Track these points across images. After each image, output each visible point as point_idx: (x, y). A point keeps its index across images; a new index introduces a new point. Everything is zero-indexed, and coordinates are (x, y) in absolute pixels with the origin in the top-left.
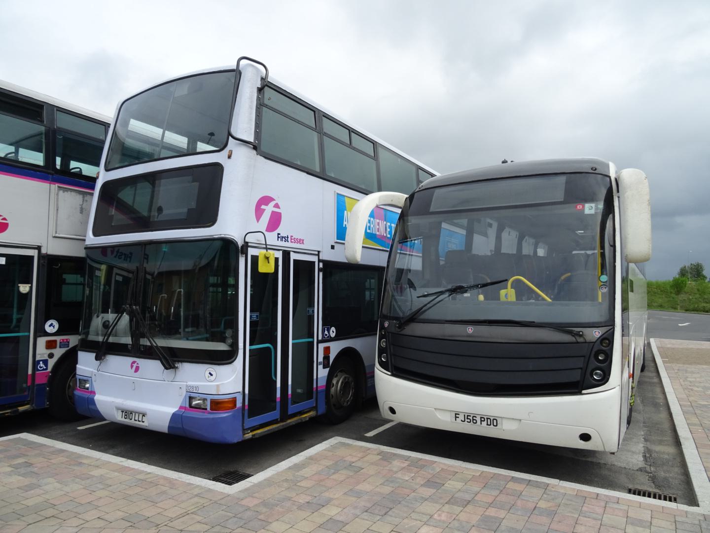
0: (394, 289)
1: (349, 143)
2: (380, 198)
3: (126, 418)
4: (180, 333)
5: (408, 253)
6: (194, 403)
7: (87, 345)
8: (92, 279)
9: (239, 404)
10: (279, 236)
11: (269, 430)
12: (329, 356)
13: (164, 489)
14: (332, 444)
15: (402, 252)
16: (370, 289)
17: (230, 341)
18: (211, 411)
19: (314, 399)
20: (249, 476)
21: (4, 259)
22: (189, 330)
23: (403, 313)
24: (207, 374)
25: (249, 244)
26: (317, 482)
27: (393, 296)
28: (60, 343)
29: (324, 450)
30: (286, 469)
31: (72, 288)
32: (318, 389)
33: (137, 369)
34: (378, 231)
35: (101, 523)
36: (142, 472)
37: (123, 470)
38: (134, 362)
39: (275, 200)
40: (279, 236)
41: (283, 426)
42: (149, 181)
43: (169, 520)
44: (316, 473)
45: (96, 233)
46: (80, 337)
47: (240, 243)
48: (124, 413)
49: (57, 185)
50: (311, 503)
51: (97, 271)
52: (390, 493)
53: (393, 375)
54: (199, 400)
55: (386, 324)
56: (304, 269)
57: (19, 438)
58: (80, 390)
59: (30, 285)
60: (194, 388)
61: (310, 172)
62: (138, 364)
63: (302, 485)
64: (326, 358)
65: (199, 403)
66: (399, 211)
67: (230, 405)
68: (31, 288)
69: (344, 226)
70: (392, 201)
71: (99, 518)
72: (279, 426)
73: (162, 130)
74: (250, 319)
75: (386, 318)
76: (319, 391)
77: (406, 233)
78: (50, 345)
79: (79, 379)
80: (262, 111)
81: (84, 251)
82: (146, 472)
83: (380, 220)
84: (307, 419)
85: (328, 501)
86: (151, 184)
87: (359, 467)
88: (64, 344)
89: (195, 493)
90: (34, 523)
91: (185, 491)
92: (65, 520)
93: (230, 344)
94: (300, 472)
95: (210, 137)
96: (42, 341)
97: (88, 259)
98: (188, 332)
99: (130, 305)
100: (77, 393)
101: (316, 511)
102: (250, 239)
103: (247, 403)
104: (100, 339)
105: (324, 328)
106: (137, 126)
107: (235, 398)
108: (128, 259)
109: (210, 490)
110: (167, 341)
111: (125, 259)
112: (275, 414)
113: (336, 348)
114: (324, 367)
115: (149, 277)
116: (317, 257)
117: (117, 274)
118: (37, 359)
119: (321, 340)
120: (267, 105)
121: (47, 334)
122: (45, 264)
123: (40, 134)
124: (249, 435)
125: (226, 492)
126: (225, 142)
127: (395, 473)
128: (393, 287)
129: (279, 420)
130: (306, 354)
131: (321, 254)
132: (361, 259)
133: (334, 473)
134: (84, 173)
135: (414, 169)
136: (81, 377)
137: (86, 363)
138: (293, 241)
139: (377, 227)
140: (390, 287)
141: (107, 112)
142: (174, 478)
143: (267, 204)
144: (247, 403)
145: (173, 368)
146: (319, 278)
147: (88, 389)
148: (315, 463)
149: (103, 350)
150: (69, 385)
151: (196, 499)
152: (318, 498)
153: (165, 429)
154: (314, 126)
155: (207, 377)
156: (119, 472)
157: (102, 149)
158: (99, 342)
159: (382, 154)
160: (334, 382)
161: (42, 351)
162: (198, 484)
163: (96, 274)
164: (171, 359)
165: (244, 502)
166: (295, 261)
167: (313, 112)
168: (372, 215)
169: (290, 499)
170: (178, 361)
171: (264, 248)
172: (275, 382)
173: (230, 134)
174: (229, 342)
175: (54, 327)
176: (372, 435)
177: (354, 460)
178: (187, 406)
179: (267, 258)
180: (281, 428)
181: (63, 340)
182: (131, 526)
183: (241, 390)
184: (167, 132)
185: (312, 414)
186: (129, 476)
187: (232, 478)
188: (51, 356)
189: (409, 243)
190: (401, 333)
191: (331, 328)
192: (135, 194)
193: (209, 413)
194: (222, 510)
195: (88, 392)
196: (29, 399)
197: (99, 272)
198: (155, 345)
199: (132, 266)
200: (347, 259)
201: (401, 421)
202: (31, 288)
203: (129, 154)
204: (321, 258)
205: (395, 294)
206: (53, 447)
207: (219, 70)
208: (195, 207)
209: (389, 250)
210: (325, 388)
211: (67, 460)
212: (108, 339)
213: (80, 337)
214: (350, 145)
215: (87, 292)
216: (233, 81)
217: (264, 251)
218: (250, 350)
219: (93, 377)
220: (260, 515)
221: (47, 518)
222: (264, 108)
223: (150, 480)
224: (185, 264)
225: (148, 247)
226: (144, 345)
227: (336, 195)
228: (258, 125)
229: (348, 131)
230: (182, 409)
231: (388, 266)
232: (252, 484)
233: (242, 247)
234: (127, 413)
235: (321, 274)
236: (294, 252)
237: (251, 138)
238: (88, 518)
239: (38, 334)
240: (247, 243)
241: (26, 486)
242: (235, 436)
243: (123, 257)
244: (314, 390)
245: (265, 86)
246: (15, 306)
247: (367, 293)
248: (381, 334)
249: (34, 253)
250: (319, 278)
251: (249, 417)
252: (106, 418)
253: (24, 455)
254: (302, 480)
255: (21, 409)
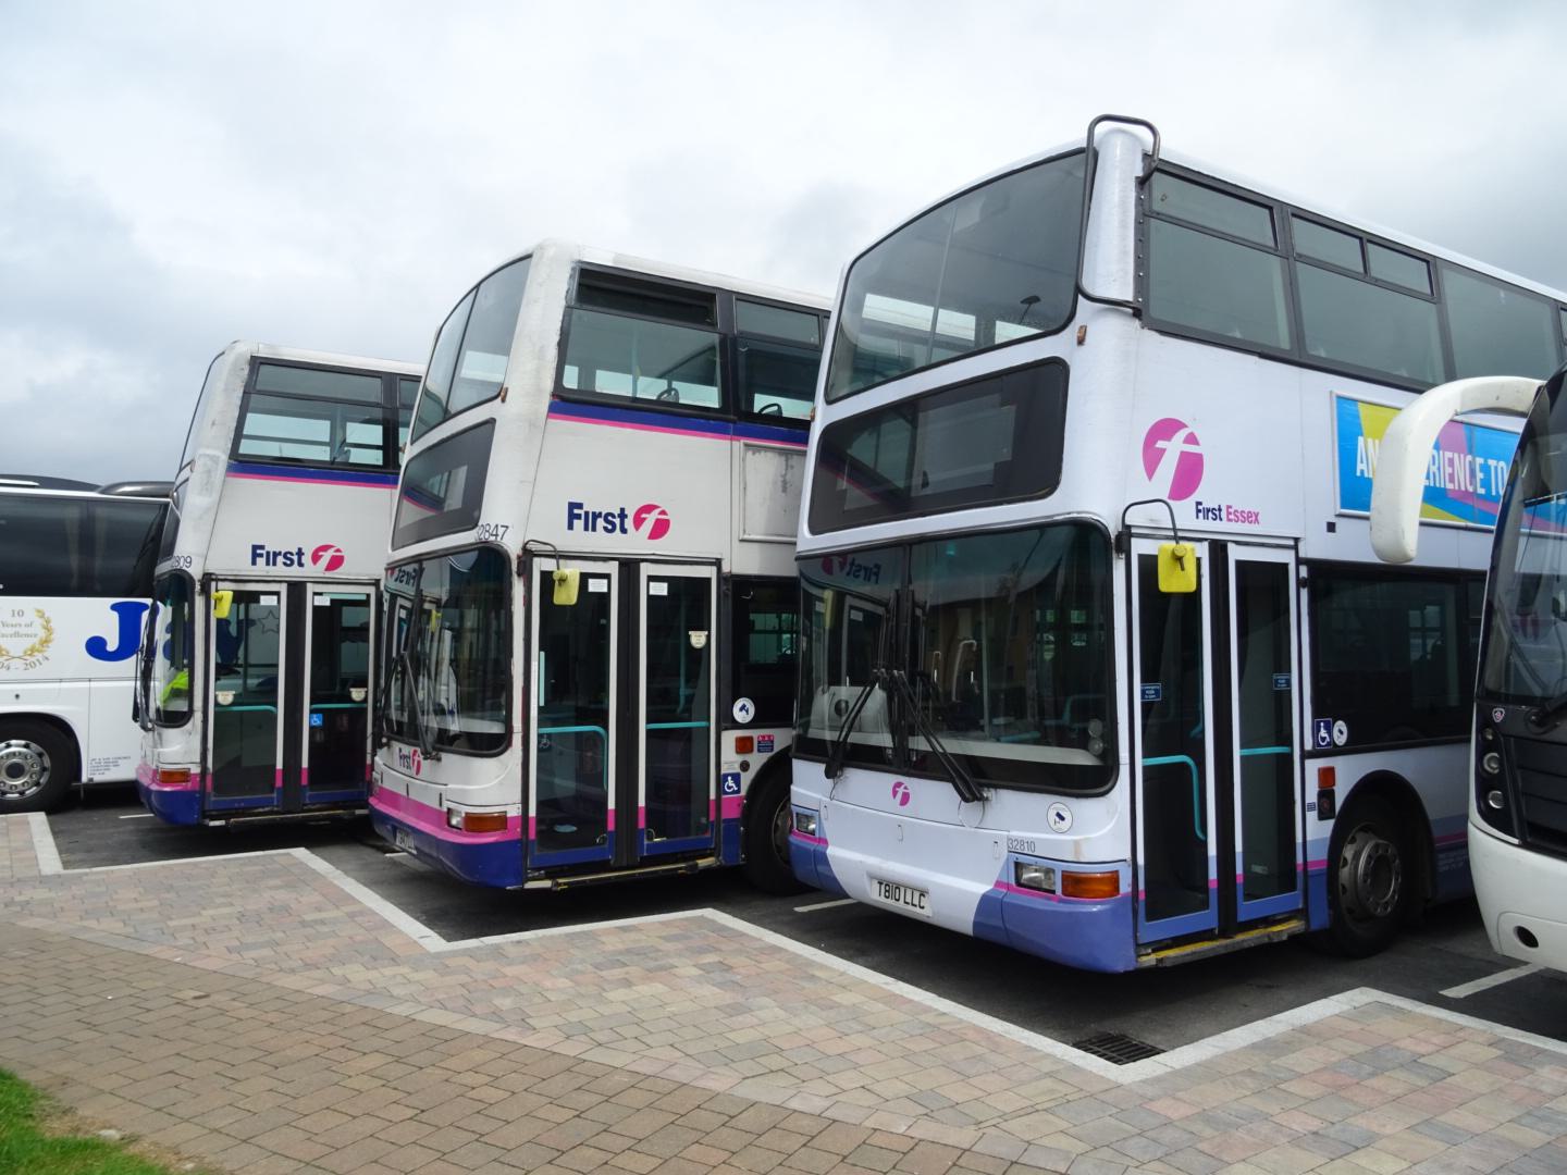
0: (1514, 626)
1: (1361, 270)
2: (1464, 394)
3: (887, 897)
4: (982, 728)
5: (1552, 533)
6: (1026, 876)
7: (810, 749)
8: (811, 621)
9: (1125, 887)
10: (1200, 507)
11: (1193, 953)
12: (1333, 792)
13: (979, 1050)
14: (1357, 1005)
15: (1533, 531)
16: (1424, 631)
17: (1098, 746)
18: (1064, 897)
19: (1298, 892)
20: (1150, 1052)
21: (665, 585)
22: (1001, 721)
23: (1544, 687)
24: (1052, 817)
25: (1134, 531)
26: (1329, 1090)
27: (1513, 644)
28: (759, 742)
29: (1337, 1015)
30: (1245, 1048)
31: (771, 640)
32: (1309, 869)
33: (905, 800)
34: (1452, 480)
35: (867, 1100)
36: (928, 1010)
37: (893, 1000)
38: (899, 785)
39: (1186, 426)
40: (1200, 507)
41: (1226, 946)
42: (904, 417)
43: (1000, 1117)
44: (1326, 1068)
45: (815, 529)
46: (794, 733)
47: (1113, 528)
48: (883, 886)
49: (742, 441)
50: (1323, 1136)
51: (817, 603)
52: (1541, 1147)
53: (1525, 845)
54: (1036, 871)
55: (1499, 715)
56: (1263, 583)
57: (702, 916)
58: (798, 835)
59: (706, 633)
60: (1026, 845)
61: (1266, 351)
62: (663, 513)
63: (1291, 1090)
64: (1326, 794)
65: (1036, 877)
66: (1519, 425)
67: (1106, 888)
68: (709, 637)
69: (1358, 474)
70: (1498, 398)
71: (863, 1087)
72: (1218, 946)
73: (932, 309)
74: (1143, 697)
75: (1494, 697)
76: (1310, 874)
77: (1546, 480)
78: (744, 746)
79: (797, 814)
80: (1149, 227)
81: (796, 563)
82: (936, 1010)
83: (1454, 451)
84: (1285, 938)
85: (1369, 1141)
86: (907, 421)
87: (1442, 1070)
88: (766, 745)
89: (1046, 1070)
90: (753, 1077)
91: (1022, 1060)
92: (804, 1081)
93: (1100, 752)
94: (1283, 1058)
95: (1026, 306)
96: (730, 738)
97: (802, 580)
98: (998, 726)
99: (889, 669)
100: (793, 839)
101: (1341, 1157)
102: (1135, 518)
103: (1141, 886)
104: (829, 736)
105: (1319, 723)
106: (881, 308)
107: (1117, 872)
108: (873, 578)
109: (1075, 1068)
110: (963, 743)
111: (867, 579)
112: (1208, 918)
113: (1350, 772)
114: (1322, 817)
115: (919, 612)
116: (1293, 552)
117: (852, 607)
118: (723, 772)
119: (1309, 752)
120: (1158, 214)
121: (736, 725)
122: (730, 593)
123: (712, 348)
124: (1149, 960)
125: (1112, 1078)
126: (1067, 314)
127: (1551, 1100)
128: (1513, 622)
129: (1217, 932)
130: (1274, 782)
131: (1301, 546)
132: (1419, 548)
133: (1373, 1075)
134: (785, 414)
135: (1547, 312)
136: (801, 810)
137: (808, 783)
138: (1232, 517)
139: (1448, 470)
140: (1504, 618)
141: (822, 292)
142: (995, 1030)
143: (1168, 437)
144: (1141, 886)
145: (979, 799)
146: (1299, 603)
147: (813, 833)
148: (1318, 1044)
149: (841, 758)
150: (776, 825)
151: (1048, 1083)
152: (1338, 1126)
153: (968, 929)
154: (1271, 243)
155: (1052, 823)
156: (884, 1003)
157: (817, 364)
158: (824, 741)
159: (1451, 285)
160: (1348, 853)
161: (730, 759)
162: (1049, 1050)
163: (817, 609)
164: (975, 780)
165: (1157, 1106)
166: (1239, 563)
167: (1267, 211)
168: (1437, 447)
169: (1267, 1117)
170: (989, 786)
171: (1168, 538)
172: (1204, 844)
173: (1079, 290)
174: (1097, 747)
175: (747, 711)
176: (1462, 996)
177: (1422, 1049)
178: (1012, 881)
179: (1179, 559)
180: (1223, 951)
181: (764, 737)
182: (926, 1115)
183: (1128, 855)
184: (942, 312)
185: (1294, 925)
186: (906, 1013)
187: (1124, 1050)
188: (745, 766)
189: (1553, 502)
190: (1547, 737)
191: (1334, 723)
192: (877, 446)
193: (1060, 901)
194: (1110, 1116)
195: (815, 840)
196: (713, 846)
197: (822, 604)
198: (941, 750)
199: (886, 590)
200: (1378, 553)
201: (1550, 967)
202: (709, 637)
203: (868, 369)
204: (1302, 555)
205: (1519, 639)
206: (760, 940)
207: (1048, 156)
208: (1010, 459)
209: (1494, 527)
210: (1325, 867)
211: (788, 966)
212: (847, 736)
213: (794, 733)
214: (1365, 275)
215: (804, 645)
216: (1082, 175)
217: (1171, 544)
218: (1146, 769)
219: (823, 812)
220: (1201, 1141)
221: (772, 1071)
222: (1152, 220)
223: (947, 1028)
224: (981, 584)
225: (915, 548)
226: (917, 751)
227: (1335, 399)
228: (1141, 262)
229: (1357, 241)
230: (1002, 887)
231: (1494, 568)
232: (1169, 1070)
233: (1119, 536)
234: (890, 887)
235: (1304, 593)
236: (1237, 543)
237: (1127, 294)
238: (845, 1086)
239: (723, 725)
240: (1129, 527)
241: (728, 1006)
242: (1119, 957)
243: (862, 573)
244: (1300, 870)
245: (1155, 169)
246: (682, 671)
247: (1416, 641)
248: (1485, 739)
249: (709, 572)
250: (1299, 603)
251: (1151, 916)
252: (850, 894)
253: (717, 950)
254: (1291, 1080)
255: (702, 863)
